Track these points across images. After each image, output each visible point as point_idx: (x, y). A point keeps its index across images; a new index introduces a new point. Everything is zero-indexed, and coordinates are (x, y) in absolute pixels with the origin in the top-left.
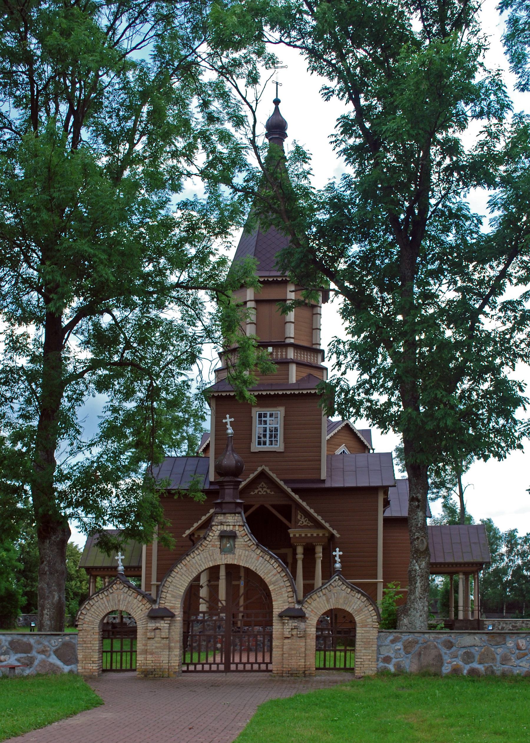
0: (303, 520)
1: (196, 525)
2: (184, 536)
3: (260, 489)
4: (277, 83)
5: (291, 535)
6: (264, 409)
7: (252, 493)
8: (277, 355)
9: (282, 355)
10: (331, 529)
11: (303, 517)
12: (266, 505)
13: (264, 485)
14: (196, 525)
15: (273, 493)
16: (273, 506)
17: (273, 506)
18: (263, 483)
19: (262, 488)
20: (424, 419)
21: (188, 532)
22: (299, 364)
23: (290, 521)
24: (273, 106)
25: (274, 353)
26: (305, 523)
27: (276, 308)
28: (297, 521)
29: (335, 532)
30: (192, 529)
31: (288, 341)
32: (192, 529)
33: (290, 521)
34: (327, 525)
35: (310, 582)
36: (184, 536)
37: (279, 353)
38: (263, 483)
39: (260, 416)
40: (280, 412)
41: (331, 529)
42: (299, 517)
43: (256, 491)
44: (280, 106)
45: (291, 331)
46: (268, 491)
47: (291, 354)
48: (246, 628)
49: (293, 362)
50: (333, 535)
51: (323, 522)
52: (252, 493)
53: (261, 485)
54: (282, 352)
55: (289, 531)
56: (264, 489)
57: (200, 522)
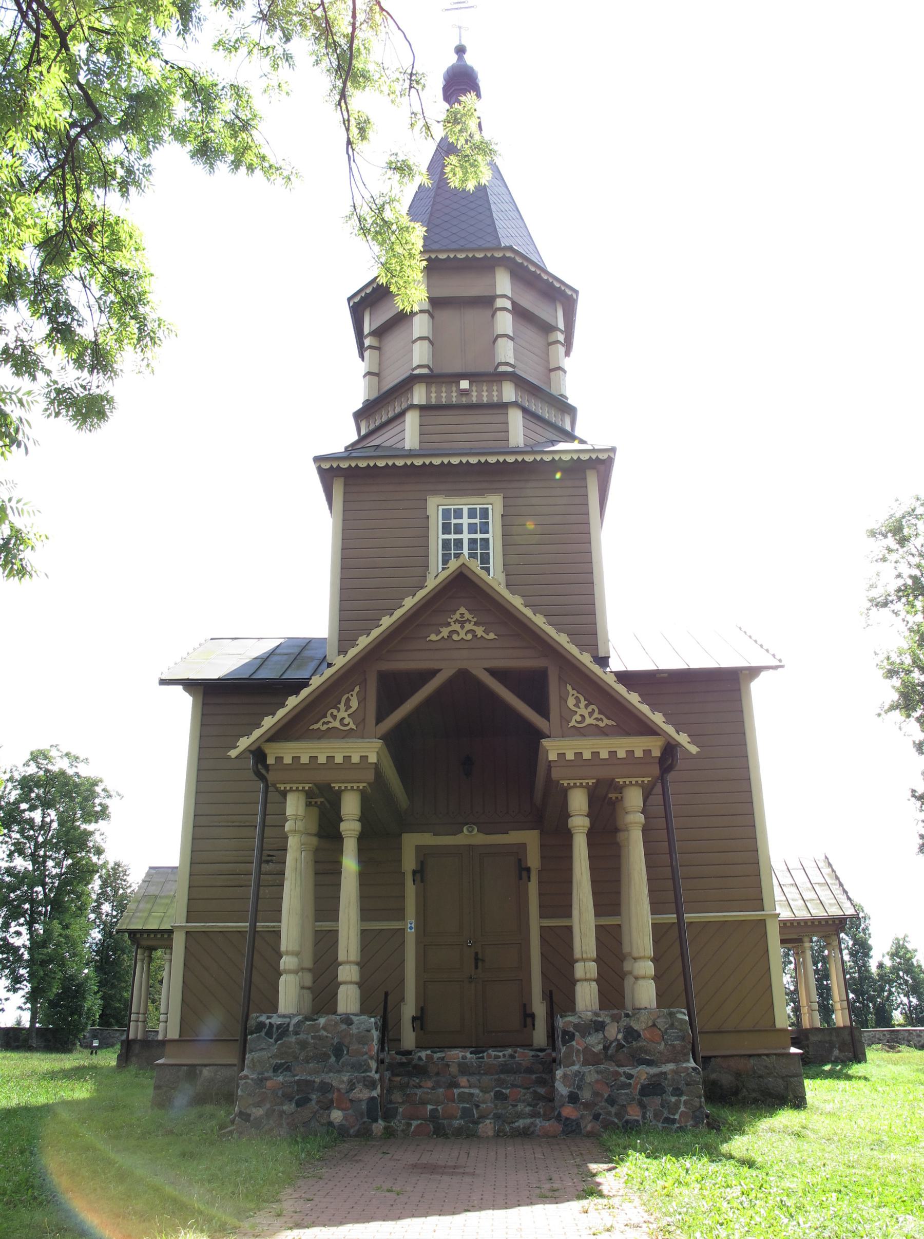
0: (582, 712)
1: (268, 722)
2: (233, 753)
3: (457, 627)
4: (460, 27)
5: (552, 756)
6: (457, 500)
7: (433, 637)
8: (480, 396)
9: (490, 395)
10: (670, 730)
11: (583, 703)
12: (474, 672)
13: (468, 615)
14: (268, 722)
15: (492, 636)
16: (497, 674)
17: (493, 672)
18: (462, 610)
19: (462, 623)
20: (274, 1037)
21: (244, 743)
22: (525, 411)
23: (544, 712)
24: (456, 57)
25: (474, 394)
26: (589, 721)
27: (472, 316)
28: (565, 719)
29: (683, 739)
30: (257, 733)
31: (502, 369)
32: (257, 733)
33: (544, 712)
34: (658, 718)
35: (326, 925)
36: (233, 753)
37: (485, 394)
38: (462, 610)
39: (446, 514)
40: (494, 504)
41: (670, 730)
42: (571, 702)
43: (445, 632)
44: (465, 56)
45: (506, 352)
46: (480, 631)
47: (509, 393)
48: (423, 1054)
49: (515, 404)
50: (670, 749)
51: (645, 709)
52: (433, 637)
53: (457, 616)
54: (490, 391)
55: (545, 742)
56: (468, 626)
57: (281, 713)
